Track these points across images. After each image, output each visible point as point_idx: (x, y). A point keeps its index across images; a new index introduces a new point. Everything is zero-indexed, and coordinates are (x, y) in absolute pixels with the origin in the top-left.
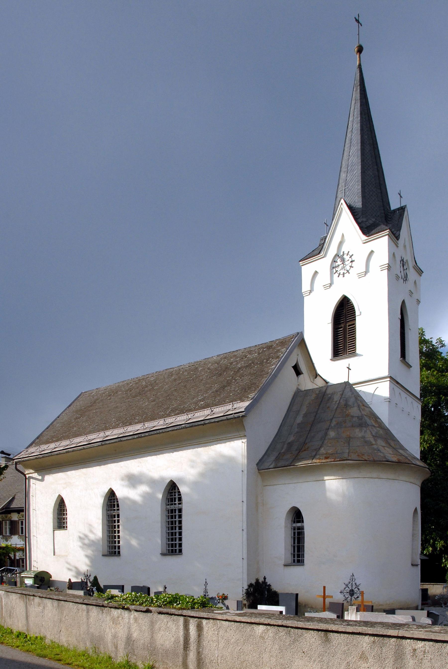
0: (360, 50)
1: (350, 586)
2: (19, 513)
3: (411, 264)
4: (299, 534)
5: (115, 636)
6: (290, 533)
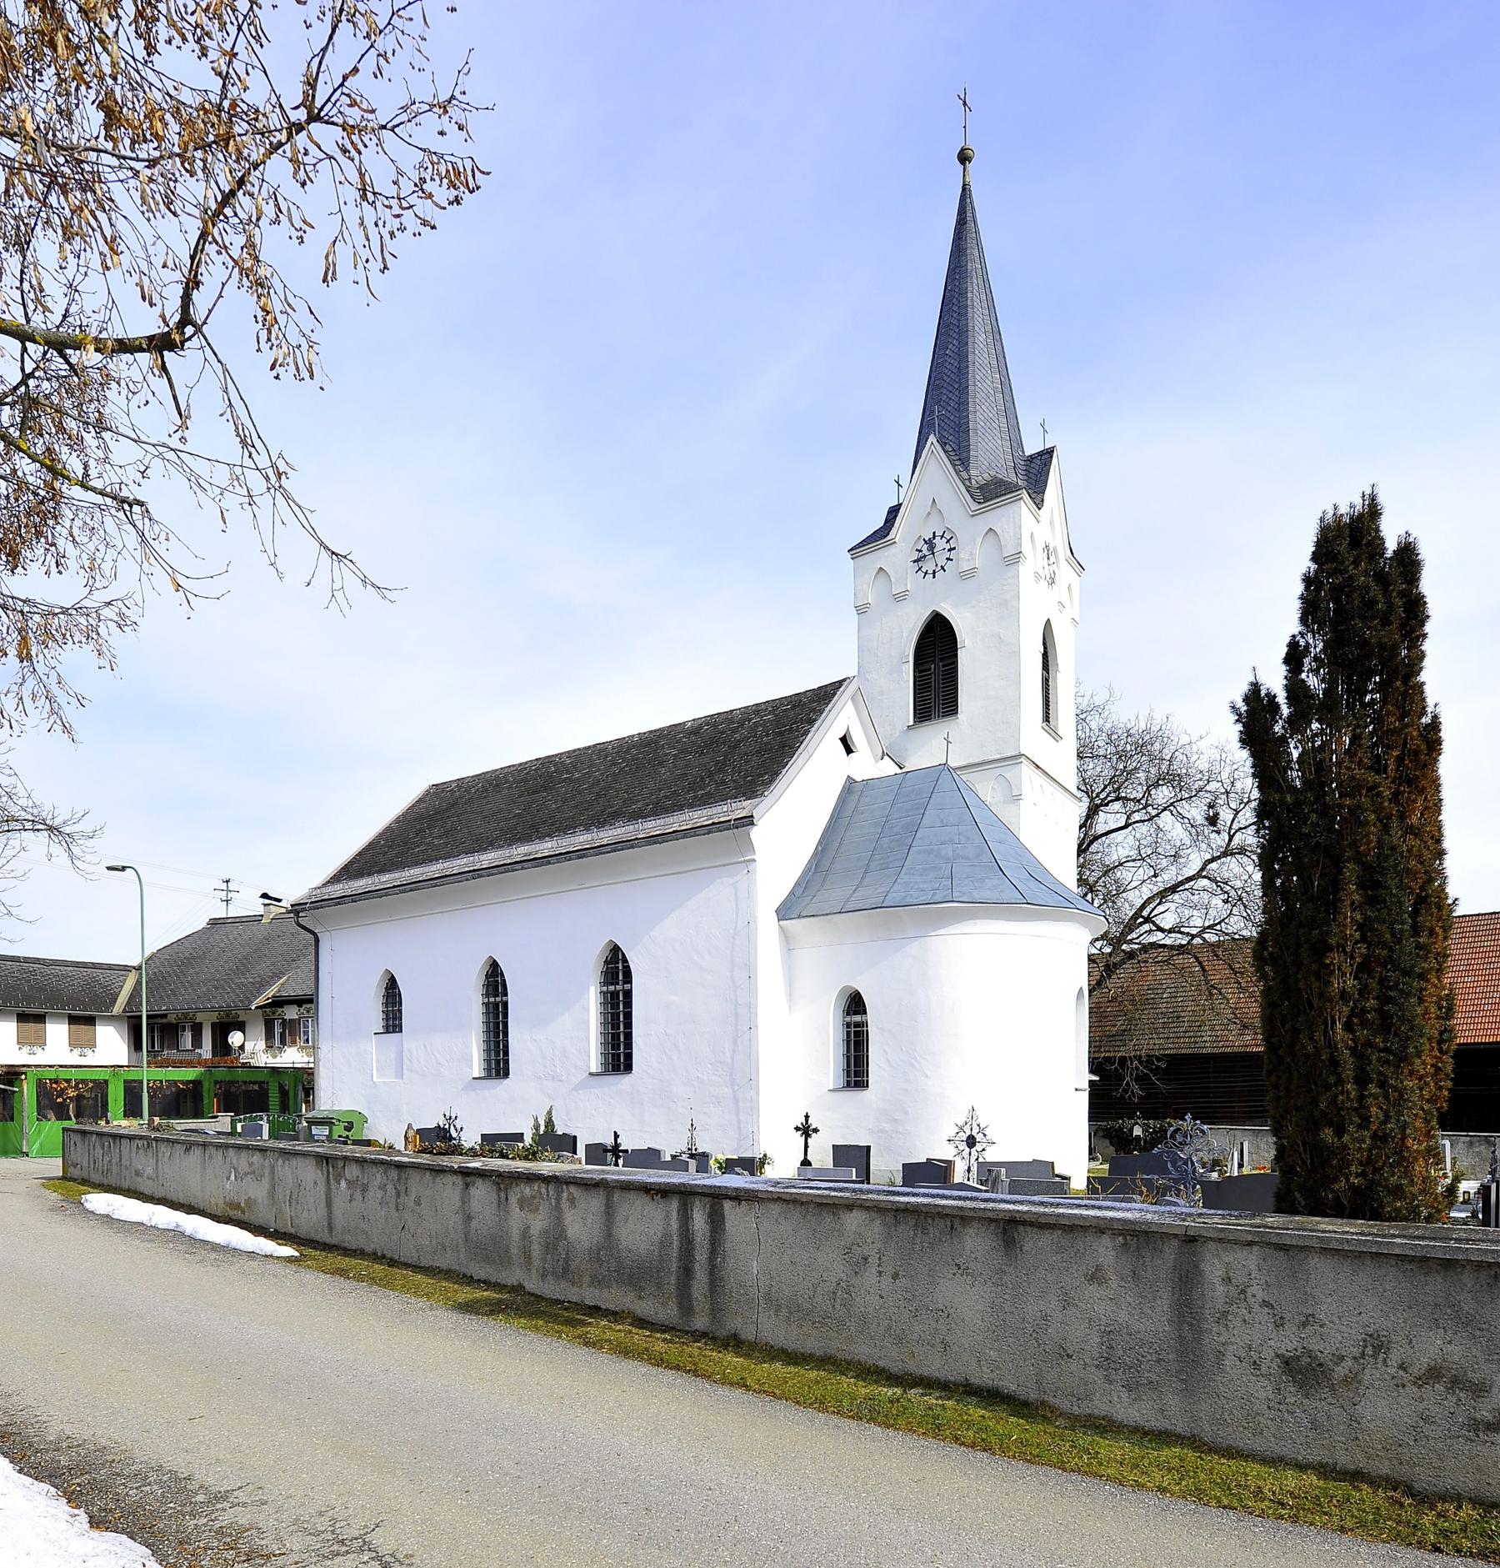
0: (964, 157)
1: (967, 1129)
2: (300, 1006)
3: (1063, 552)
4: (857, 1034)
5: (525, 1234)
6: (841, 1034)
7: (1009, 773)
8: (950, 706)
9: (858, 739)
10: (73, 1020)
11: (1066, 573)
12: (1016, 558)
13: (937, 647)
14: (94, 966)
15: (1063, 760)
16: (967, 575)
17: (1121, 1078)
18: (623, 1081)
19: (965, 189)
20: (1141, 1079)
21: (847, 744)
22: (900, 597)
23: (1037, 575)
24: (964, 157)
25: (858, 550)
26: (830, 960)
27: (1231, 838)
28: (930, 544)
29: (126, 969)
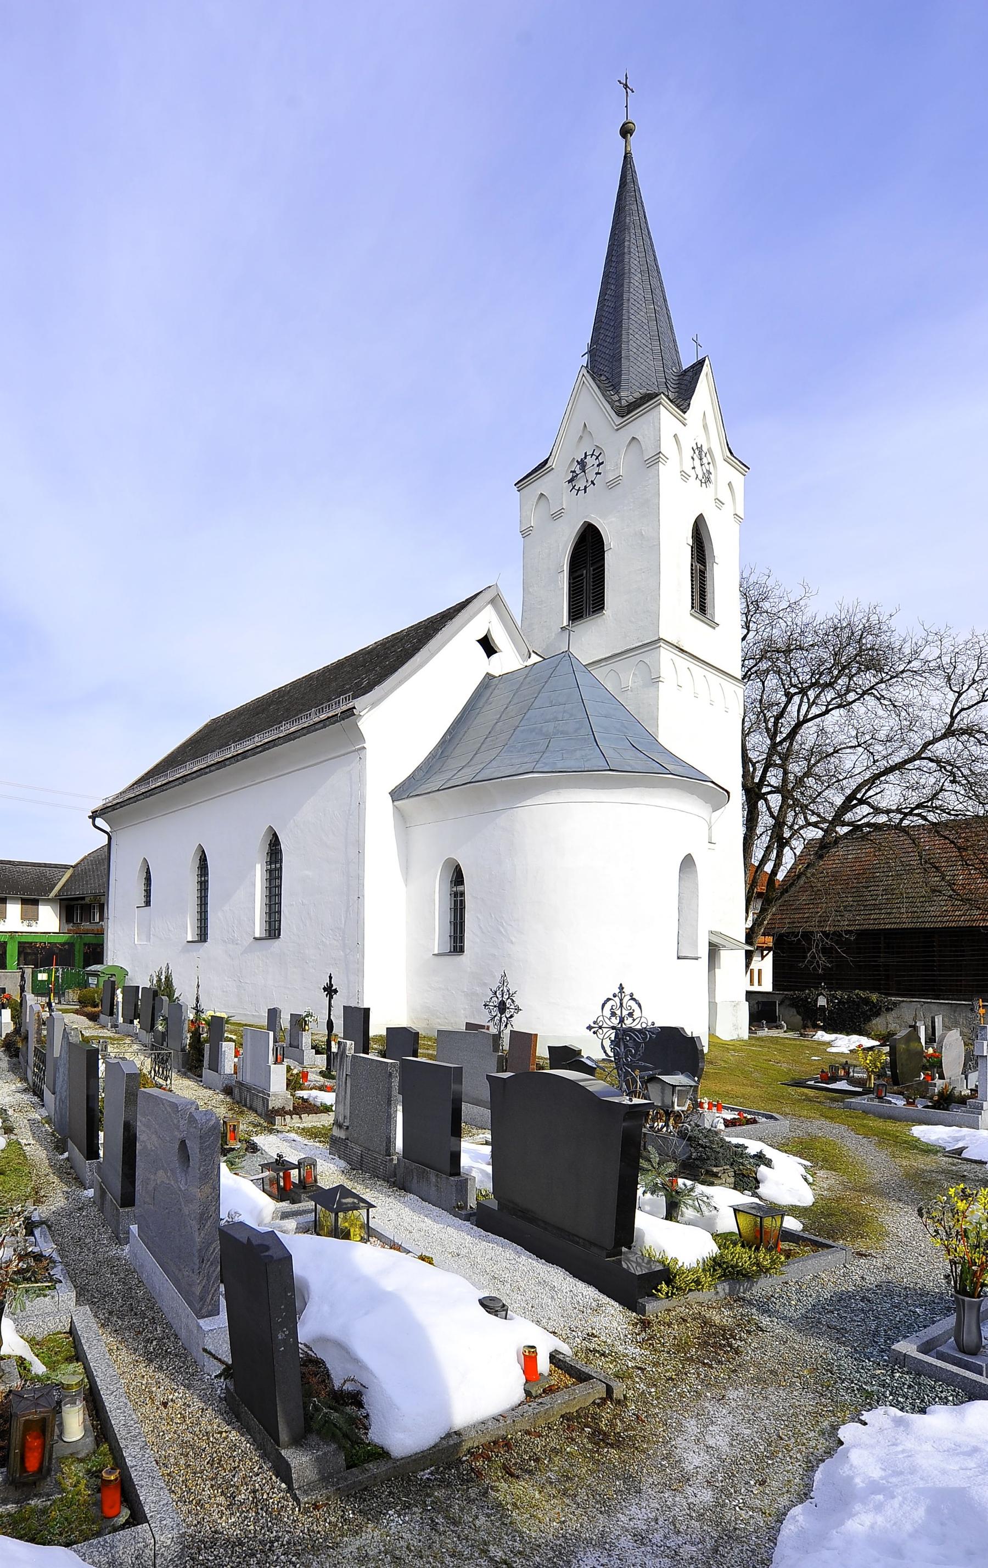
0: (626, 131)
7: (647, 658)
8: (598, 604)
9: (500, 638)
10: (24, 902)
11: (725, 472)
12: (657, 458)
13: (589, 551)
14: (46, 865)
15: (725, 642)
16: (613, 484)
17: (805, 951)
18: (276, 944)
19: (627, 158)
20: (826, 951)
21: (488, 646)
22: (557, 516)
23: (684, 476)
24: (626, 131)
25: (521, 484)
26: (443, 833)
27: (953, 718)
28: (582, 464)
29: (66, 867)
